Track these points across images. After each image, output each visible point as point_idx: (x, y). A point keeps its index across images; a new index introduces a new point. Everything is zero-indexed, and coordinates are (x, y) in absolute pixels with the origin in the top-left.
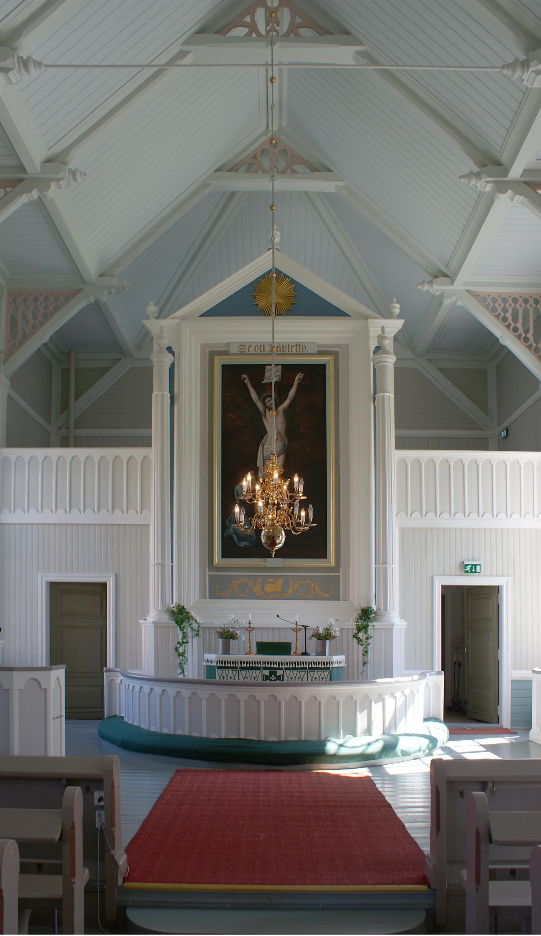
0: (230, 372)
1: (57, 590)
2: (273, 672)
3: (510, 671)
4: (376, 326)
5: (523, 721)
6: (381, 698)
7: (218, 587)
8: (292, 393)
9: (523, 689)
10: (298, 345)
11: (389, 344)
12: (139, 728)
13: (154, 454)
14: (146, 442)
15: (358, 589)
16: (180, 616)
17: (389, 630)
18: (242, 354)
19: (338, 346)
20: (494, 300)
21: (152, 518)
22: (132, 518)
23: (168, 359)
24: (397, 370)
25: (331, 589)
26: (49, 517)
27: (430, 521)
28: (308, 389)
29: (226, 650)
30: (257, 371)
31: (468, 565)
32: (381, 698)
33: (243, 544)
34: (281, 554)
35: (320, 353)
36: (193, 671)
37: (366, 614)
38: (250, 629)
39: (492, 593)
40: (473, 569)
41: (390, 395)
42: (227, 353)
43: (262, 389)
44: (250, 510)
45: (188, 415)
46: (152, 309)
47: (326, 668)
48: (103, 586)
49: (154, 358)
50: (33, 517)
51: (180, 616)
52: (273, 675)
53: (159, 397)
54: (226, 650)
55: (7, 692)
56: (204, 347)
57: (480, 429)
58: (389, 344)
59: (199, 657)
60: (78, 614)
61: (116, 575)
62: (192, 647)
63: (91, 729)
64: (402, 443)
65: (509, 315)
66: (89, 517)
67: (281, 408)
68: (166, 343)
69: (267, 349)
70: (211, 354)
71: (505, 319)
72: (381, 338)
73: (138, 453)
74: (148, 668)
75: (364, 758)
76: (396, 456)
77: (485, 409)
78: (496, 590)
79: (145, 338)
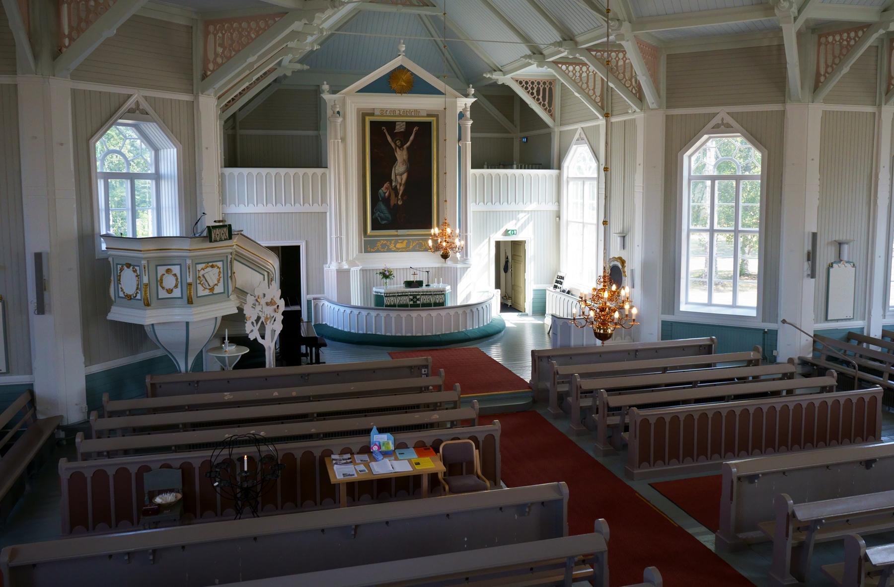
0: (376, 127)
8: (412, 138)
10: (416, 111)
11: (468, 114)
12: (337, 330)
18: (382, 115)
19: (438, 111)
20: (527, 83)
26: (260, 209)
28: (420, 136)
30: (391, 125)
33: (384, 222)
35: (429, 115)
42: (372, 114)
43: (394, 136)
56: (358, 110)
57: (509, 133)
61: (307, 242)
65: (535, 91)
67: (405, 146)
69: (397, 113)
70: (363, 115)
71: (532, 94)
76: (472, 173)
77: (512, 121)
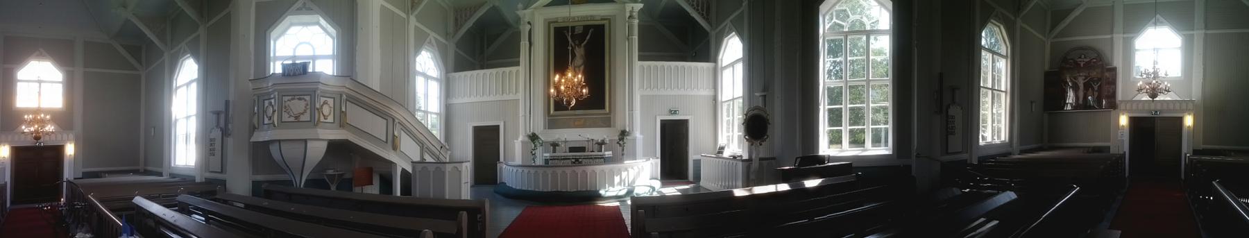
1: (478, 131)
2: (577, 160)
3: (692, 156)
4: (629, 7)
5: (697, 178)
6: (626, 170)
7: (552, 124)
9: (697, 163)
11: (635, 14)
13: (522, 69)
14: (518, 64)
15: (620, 121)
16: (533, 137)
17: (634, 140)
21: (520, 96)
22: (511, 97)
23: (528, 27)
24: (639, 26)
25: (607, 122)
27: (655, 92)
29: (554, 151)
31: (573, 108)
32: (626, 170)
34: (573, 108)
36: (539, 162)
37: (623, 134)
38: (566, 142)
39: (684, 123)
40: (675, 112)
41: (636, 37)
44: (557, 88)
45: (538, 49)
46: (520, 6)
47: (602, 157)
48: (498, 127)
49: (521, 27)
50: (466, 100)
51: (533, 137)
52: (577, 162)
53: (524, 44)
54: (554, 151)
55: (444, 173)
58: (635, 14)
59: (542, 155)
60: (487, 139)
62: (539, 151)
63: (489, 189)
64: (641, 58)
66: (492, 98)
68: (527, 20)
72: (631, 12)
73: (514, 69)
74: (518, 160)
75: (617, 198)
76: (638, 64)
78: (686, 121)
79: (518, 20)
